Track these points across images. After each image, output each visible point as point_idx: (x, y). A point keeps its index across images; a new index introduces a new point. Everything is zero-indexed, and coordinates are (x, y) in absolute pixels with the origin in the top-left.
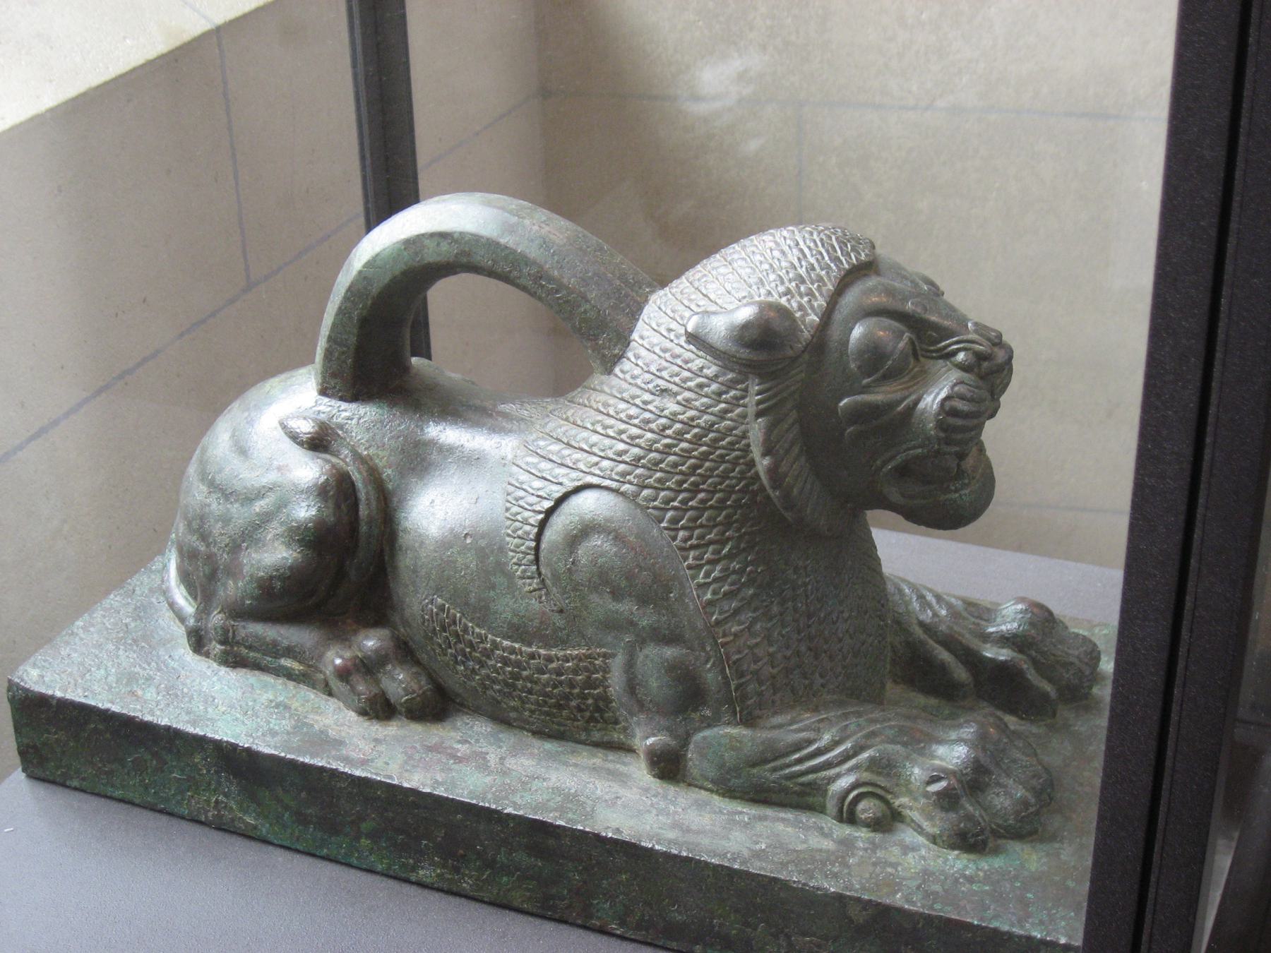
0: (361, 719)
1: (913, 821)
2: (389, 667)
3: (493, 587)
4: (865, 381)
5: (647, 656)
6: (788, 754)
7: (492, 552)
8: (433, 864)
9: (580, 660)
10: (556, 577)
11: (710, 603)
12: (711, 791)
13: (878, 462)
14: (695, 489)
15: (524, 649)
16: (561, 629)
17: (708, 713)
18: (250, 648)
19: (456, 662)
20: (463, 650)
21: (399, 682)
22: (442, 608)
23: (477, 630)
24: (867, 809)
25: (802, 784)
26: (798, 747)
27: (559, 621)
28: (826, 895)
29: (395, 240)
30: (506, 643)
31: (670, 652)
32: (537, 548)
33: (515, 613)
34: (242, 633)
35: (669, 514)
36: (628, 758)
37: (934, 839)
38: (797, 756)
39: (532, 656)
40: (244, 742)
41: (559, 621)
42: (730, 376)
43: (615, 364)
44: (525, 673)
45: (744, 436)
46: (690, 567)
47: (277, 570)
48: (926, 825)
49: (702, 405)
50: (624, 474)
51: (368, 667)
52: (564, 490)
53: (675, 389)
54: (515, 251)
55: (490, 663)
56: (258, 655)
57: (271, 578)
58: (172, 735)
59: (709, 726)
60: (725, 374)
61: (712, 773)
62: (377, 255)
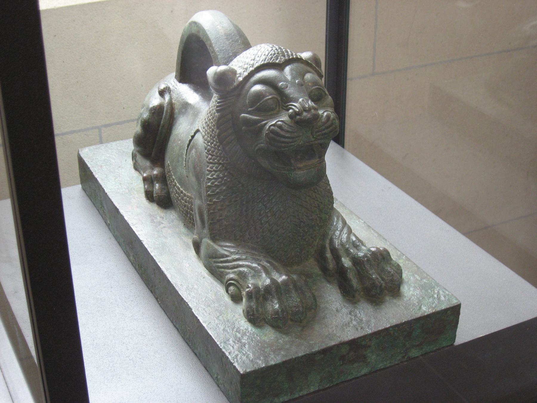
4: (250, 109)
11: (209, 187)
38: (222, 260)
46: (208, 170)
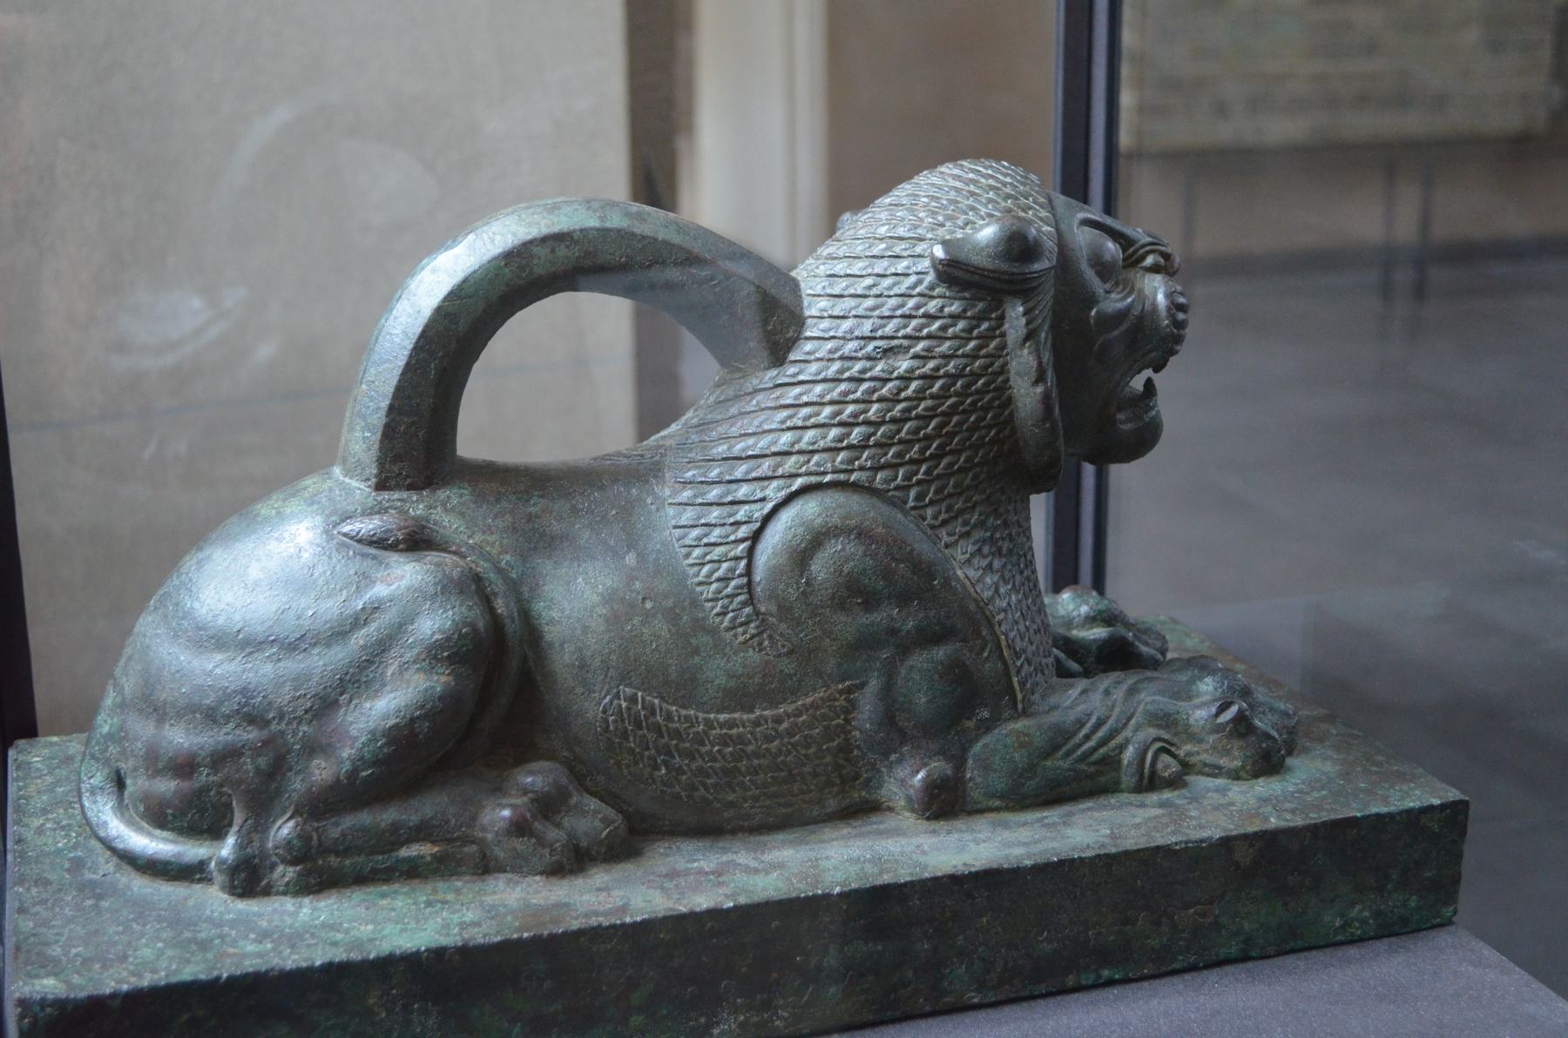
0: (553, 880)
1: (1205, 765)
2: (574, 800)
3: (696, 651)
5: (912, 667)
6: (1075, 734)
7: (683, 609)
8: (736, 1010)
9: (817, 708)
10: (785, 610)
12: (997, 809)
13: (1117, 376)
14: (937, 457)
15: (745, 717)
16: (790, 676)
17: (985, 714)
18: (347, 852)
19: (656, 767)
20: (667, 746)
21: (591, 818)
22: (633, 700)
23: (683, 712)
24: (1168, 767)
25: (1095, 763)
26: (1080, 724)
27: (787, 666)
28: (1212, 845)
29: (486, 258)
30: (723, 717)
31: (941, 653)
32: (750, 584)
33: (731, 675)
34: (334, 833)
35: (913, 493)
36: (890, 822)
37: (1235, 776)
39: (757, 723)
40: (451, 939)
41: (787, 666)
42: (980, 306)
43: (789, 350)
44: (750, 748)
45: (1003, 370)
47: (423, 707)
48: (1223, 762)
49: (950, 348)
50: (851, 461)
51: (549, 806)
52: (770, 506)
53: (905, 343)
54: (656, 240)
55: (703, 750)
56: (361, 859)
57: (413, 720)
58: (336, 973)
59: (988, 730)
60: (974, 306)
61: (999, 782)
62: (465, 281)
